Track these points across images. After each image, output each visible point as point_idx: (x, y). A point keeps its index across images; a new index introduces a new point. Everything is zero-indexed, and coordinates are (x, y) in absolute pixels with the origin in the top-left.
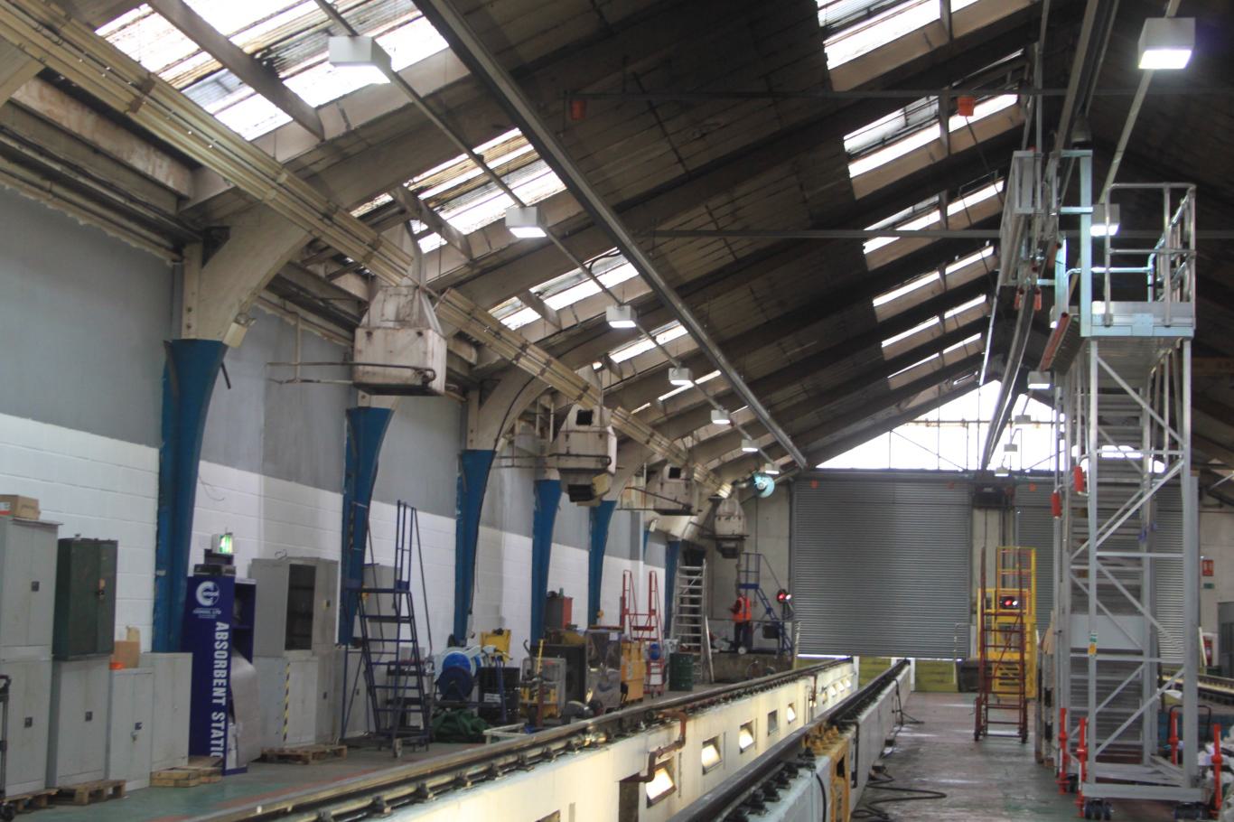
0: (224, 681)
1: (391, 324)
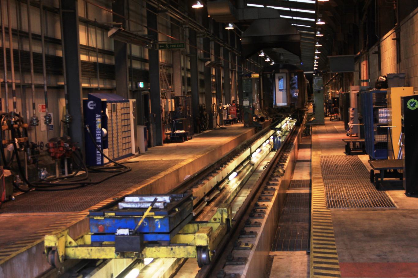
0: (100, 134)
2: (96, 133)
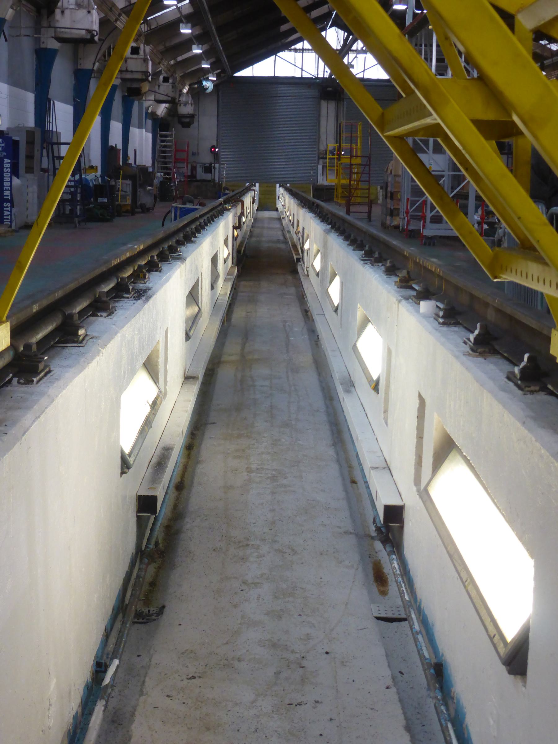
0: (9, 188)
1: (73, 7)
2: (4, 168)
